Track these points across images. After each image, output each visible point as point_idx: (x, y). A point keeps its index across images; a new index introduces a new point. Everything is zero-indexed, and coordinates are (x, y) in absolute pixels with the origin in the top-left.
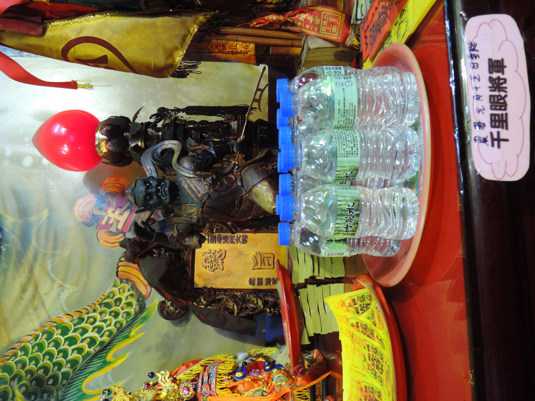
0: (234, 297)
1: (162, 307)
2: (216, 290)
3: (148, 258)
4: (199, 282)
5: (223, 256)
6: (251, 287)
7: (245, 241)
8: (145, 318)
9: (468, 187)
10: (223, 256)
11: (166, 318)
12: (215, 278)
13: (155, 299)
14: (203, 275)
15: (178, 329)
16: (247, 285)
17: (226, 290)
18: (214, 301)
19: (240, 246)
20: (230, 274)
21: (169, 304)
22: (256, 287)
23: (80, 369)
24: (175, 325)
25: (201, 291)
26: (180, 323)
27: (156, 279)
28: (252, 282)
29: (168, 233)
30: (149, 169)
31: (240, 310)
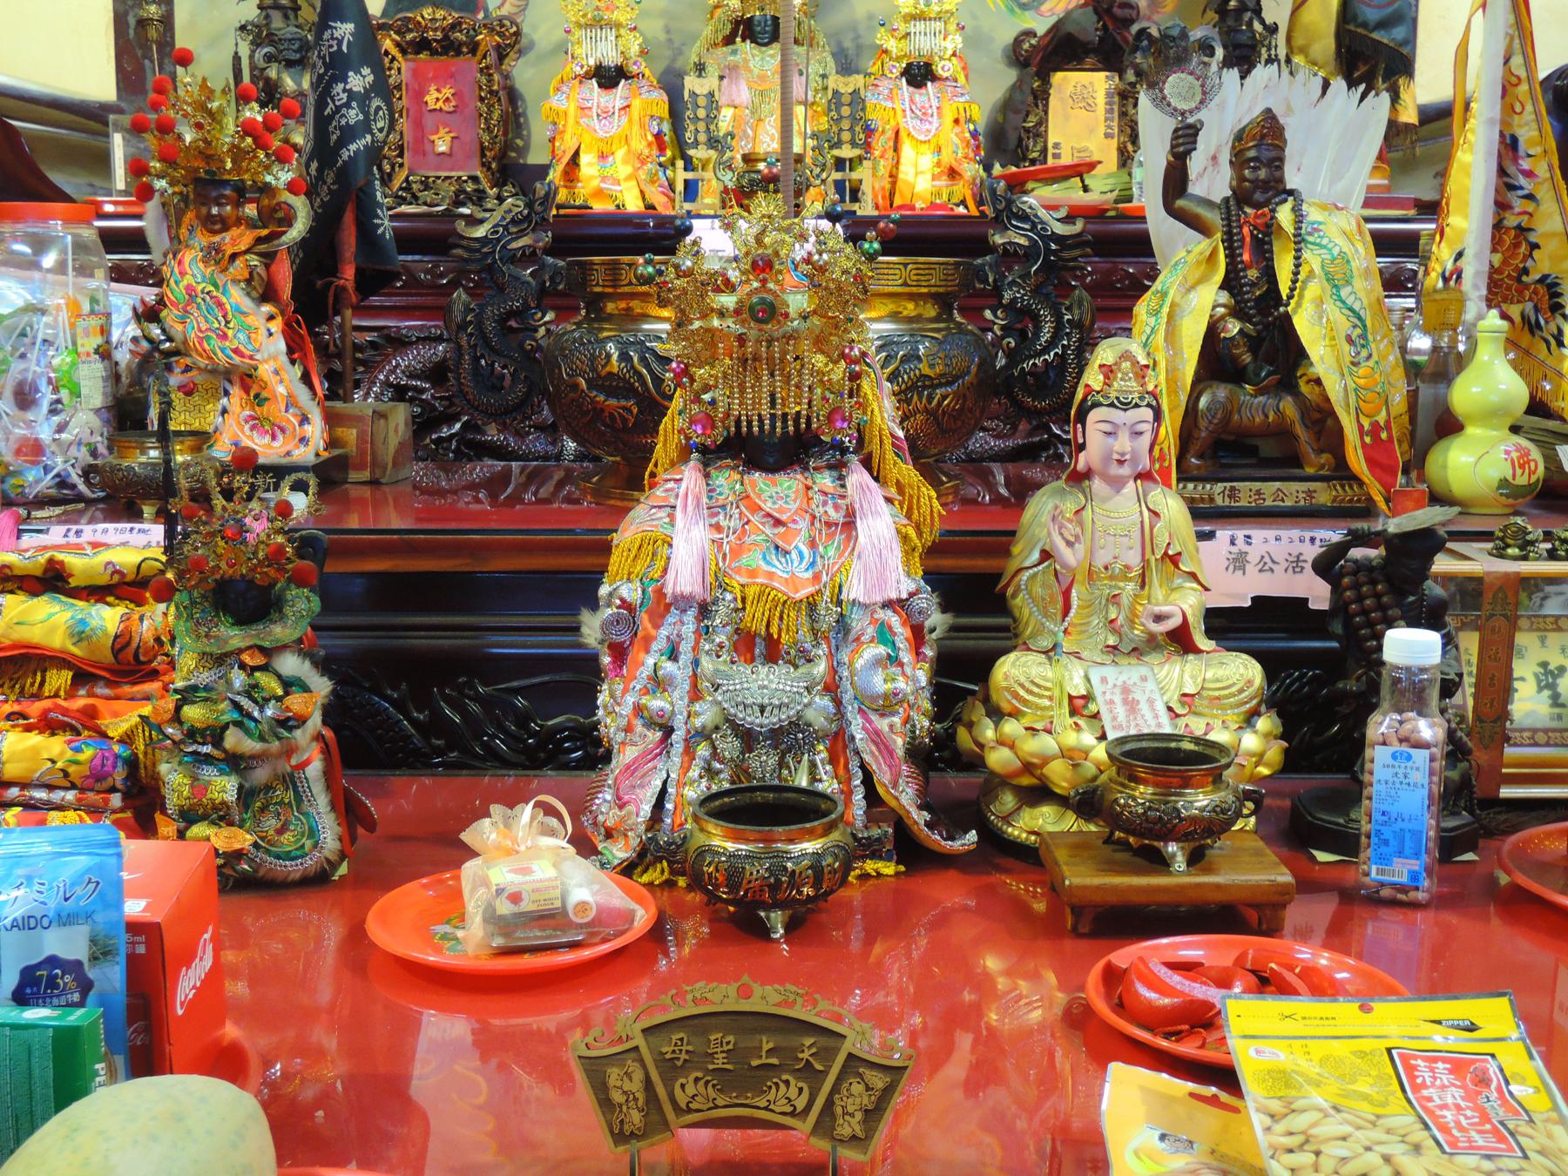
0: (1039, 123)
1: (1030, 33)
2: (1047, 100)
3: (1095, 18)
4: (1058, 78)
5: (1089, 108)
6: (1050, 145)
7: (1107, 136)
8: (1012, 11)
9: (1173, 334)
10: (1089, 108)
11: (1016, 39)
12: (1062, 100)
13: (1041, 25)
14: (1066, 82)
15: (999, 53)
16: (1051, 141)
17: (1046, 113)
18: (1036, 97)
19: (1102, 130)
20: (1067, 117)
21: (1033, 41)
22: (1051, 151)
24: (1005, 50)
25: (1046, 82)
26: (1008, 57)
27: (1070, 28)
28: (1056, 145)
29: (1138, 55)
30: (1197, 34)
31: (1027, 130)
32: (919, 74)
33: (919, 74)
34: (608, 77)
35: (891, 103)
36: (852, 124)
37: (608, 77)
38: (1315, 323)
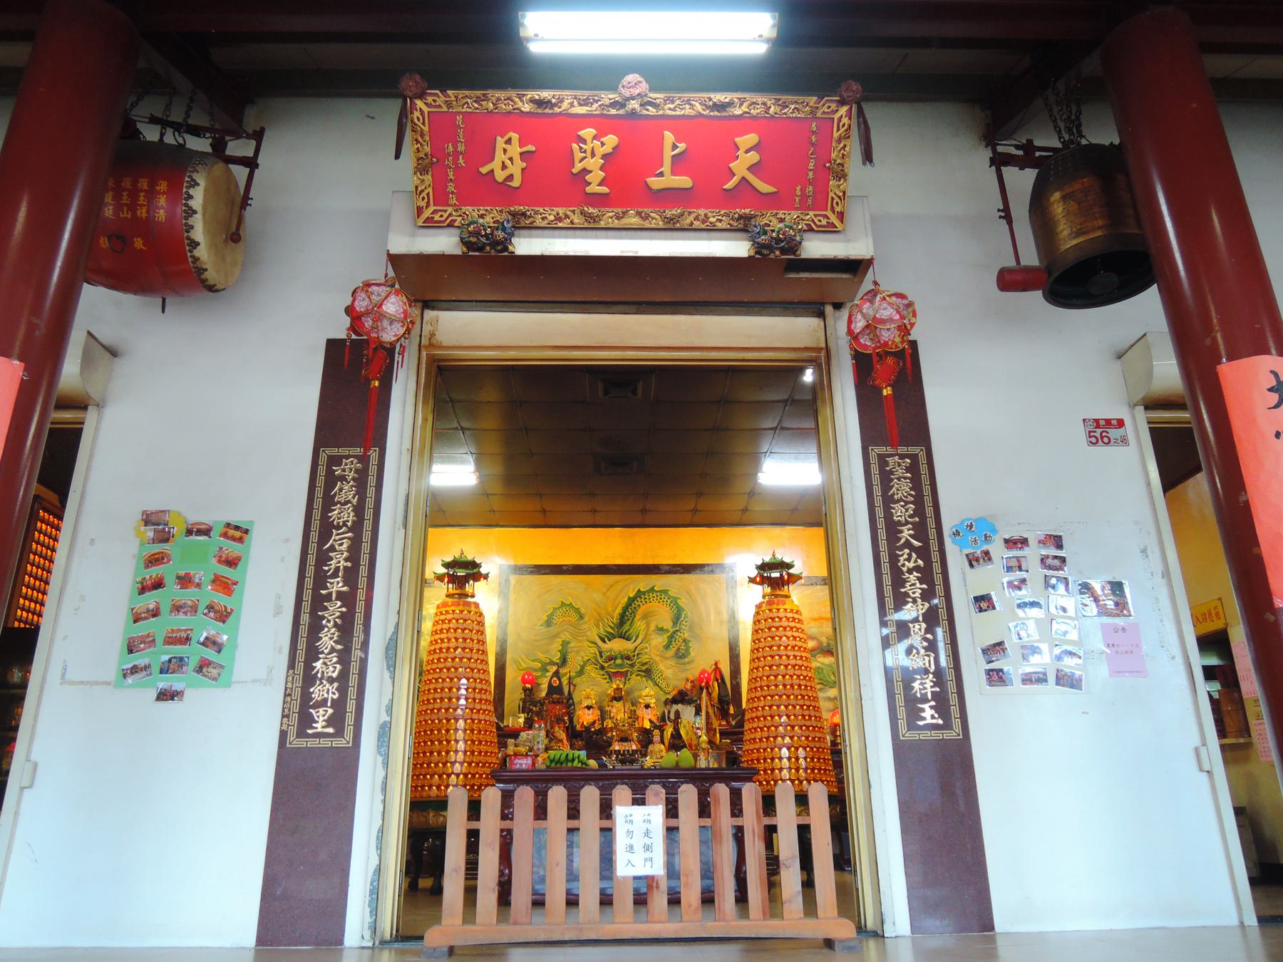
23: (653, 680)
32: (647, 706)
33: (647, 706)
34: (589, 708)
35: (641, 712)
36: (634, 716)
37: (589, 708)
38: (683, 733)
